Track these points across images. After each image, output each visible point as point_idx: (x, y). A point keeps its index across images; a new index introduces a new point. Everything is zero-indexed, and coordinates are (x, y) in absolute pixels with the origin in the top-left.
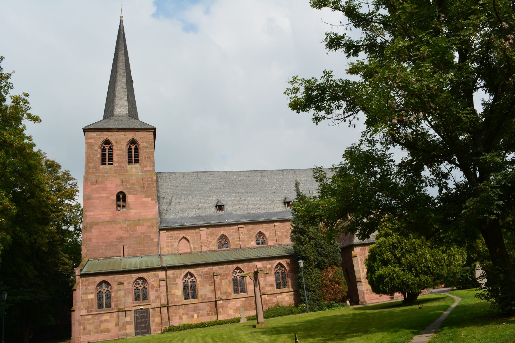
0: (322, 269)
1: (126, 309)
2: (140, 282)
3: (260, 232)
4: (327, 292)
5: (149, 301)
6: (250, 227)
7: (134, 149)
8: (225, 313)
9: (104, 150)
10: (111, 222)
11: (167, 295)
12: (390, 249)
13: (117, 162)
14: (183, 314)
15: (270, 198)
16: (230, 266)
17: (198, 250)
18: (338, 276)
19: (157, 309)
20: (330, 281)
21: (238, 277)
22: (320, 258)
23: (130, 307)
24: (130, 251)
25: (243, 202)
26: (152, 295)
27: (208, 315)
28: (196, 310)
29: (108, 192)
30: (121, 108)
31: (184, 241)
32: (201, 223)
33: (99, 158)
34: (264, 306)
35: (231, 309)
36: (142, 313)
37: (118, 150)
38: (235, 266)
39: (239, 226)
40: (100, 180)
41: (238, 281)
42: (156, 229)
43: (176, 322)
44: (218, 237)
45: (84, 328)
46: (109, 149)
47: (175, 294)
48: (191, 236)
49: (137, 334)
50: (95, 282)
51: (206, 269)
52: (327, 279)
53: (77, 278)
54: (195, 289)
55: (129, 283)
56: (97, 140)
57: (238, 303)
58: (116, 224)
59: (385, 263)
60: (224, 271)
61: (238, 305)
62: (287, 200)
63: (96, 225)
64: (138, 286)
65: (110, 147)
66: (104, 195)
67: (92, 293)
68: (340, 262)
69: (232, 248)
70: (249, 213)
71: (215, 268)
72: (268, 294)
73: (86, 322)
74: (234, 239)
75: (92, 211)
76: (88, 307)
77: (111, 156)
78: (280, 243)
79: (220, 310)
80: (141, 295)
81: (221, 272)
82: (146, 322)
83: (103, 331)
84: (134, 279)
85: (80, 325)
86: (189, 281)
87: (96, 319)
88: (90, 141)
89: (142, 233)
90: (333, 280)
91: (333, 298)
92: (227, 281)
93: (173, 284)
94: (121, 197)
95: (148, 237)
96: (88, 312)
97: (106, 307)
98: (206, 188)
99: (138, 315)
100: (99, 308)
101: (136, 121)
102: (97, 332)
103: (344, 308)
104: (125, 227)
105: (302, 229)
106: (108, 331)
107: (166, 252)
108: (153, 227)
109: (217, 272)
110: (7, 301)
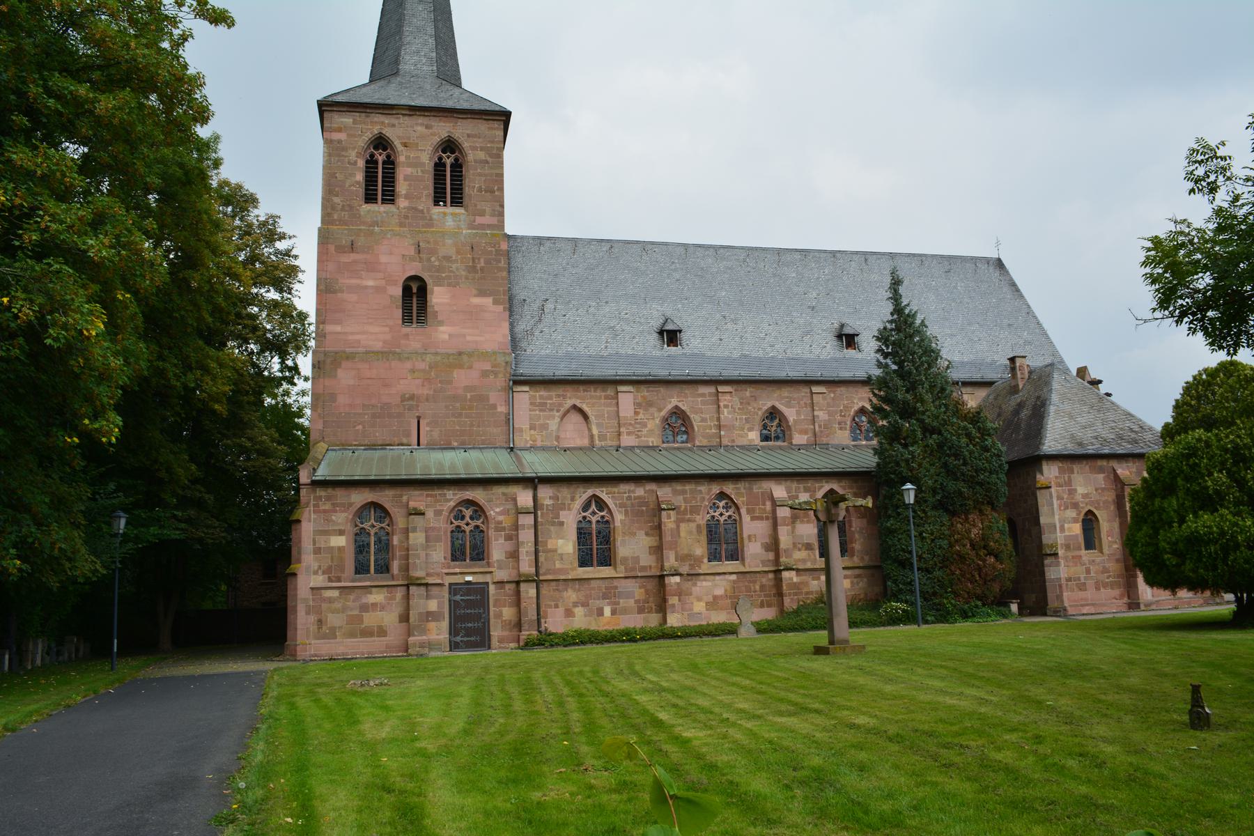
0: (953, 514)
1: (430, 580)
2: (468, 513)
3: (773, 407)
4: (963, 576)
5: (489, 564)
6: (748, 392)
7: (452, 166)
8: (683, 609)
9: (371, 163)
10: (385, 355)
11: (536, 552)
12: (1223, 463)
13: (407, 197)
14: (575, 605)
15: (802, 321)
16: (703, 488)
17: (609, 443)
18: (997, 536)
19: (508, 586)
20: (973, 545)
21: (722, 519)
22: (951, 486)
23: (438, 575)
24: (436, 434)
25: (729, 326)
26: (498, 550)
27: (641, 610)
28: (610, 594)
29: (381, 275)
30: (417, 55)
31: (575, 418)
32: (623, 372)
33: (358, 183)
34: (787, 601)
35: (699, 599)
36: (468, 592)
37: (410, 165)
38: (716, 489)
39: (721, 389)
40: (361, 241)
41: (722, 529)
42: (501, 381)
43: (556, 623)
44: (663, 413)
45: (320, 621)
46: (384, 163)
47: (555, 551)
48: (593, 405)
49: (454, 646)
50: (351, 505)
51: (640, 491)
52: (966, 542)
53: (303, 492)
54: (608, 542)
55: (438, 513)
56: (354, 136)
57: (719, 587)
58: (400, 359)
59: (1209, 502)
60: (685, 499)
61: (719, 592)
62: (847, 330)
63: (347, 358)
64: (462, 524)
65: (388, 156)
66: (371, 283)
67: (341, 533)
68: (1003, 500)
69: (697, 443)
70: (746, 356)
71: (665, 492)
72: (798, 570)
73: (324, 606)
74: (703, 420)
75: (339, 322)
76: (330, 567)
77: (390, 179)
78: (825, 440)
79: (673, 600)
80: (470, 548)
81: (679, 501)
82: (478, 617)
83: (367, 633)
84: (452, 504)
85: (308, 613)
86: (594, 519)
87: (351, 601)
88: (336, 136)
89: (467, 388)
90: (983, 546)
91: (979, 591)
92: (693, 526)
93: (553, 524)
94: (415, 297)
95: (482, 399)
96: (330, 580)
97: (377, 571)
98: (633, 283)
99: (458, 598)
100: (357, 571)
101: (457, 91)
102: (352, 635)
103: (1004, 621)
104: (423, 371)
105: (905, 402)
106: (382, 632)
107: (526, 441)
108: (496, 374)
109: (668, 502)
110: (126, 538)
